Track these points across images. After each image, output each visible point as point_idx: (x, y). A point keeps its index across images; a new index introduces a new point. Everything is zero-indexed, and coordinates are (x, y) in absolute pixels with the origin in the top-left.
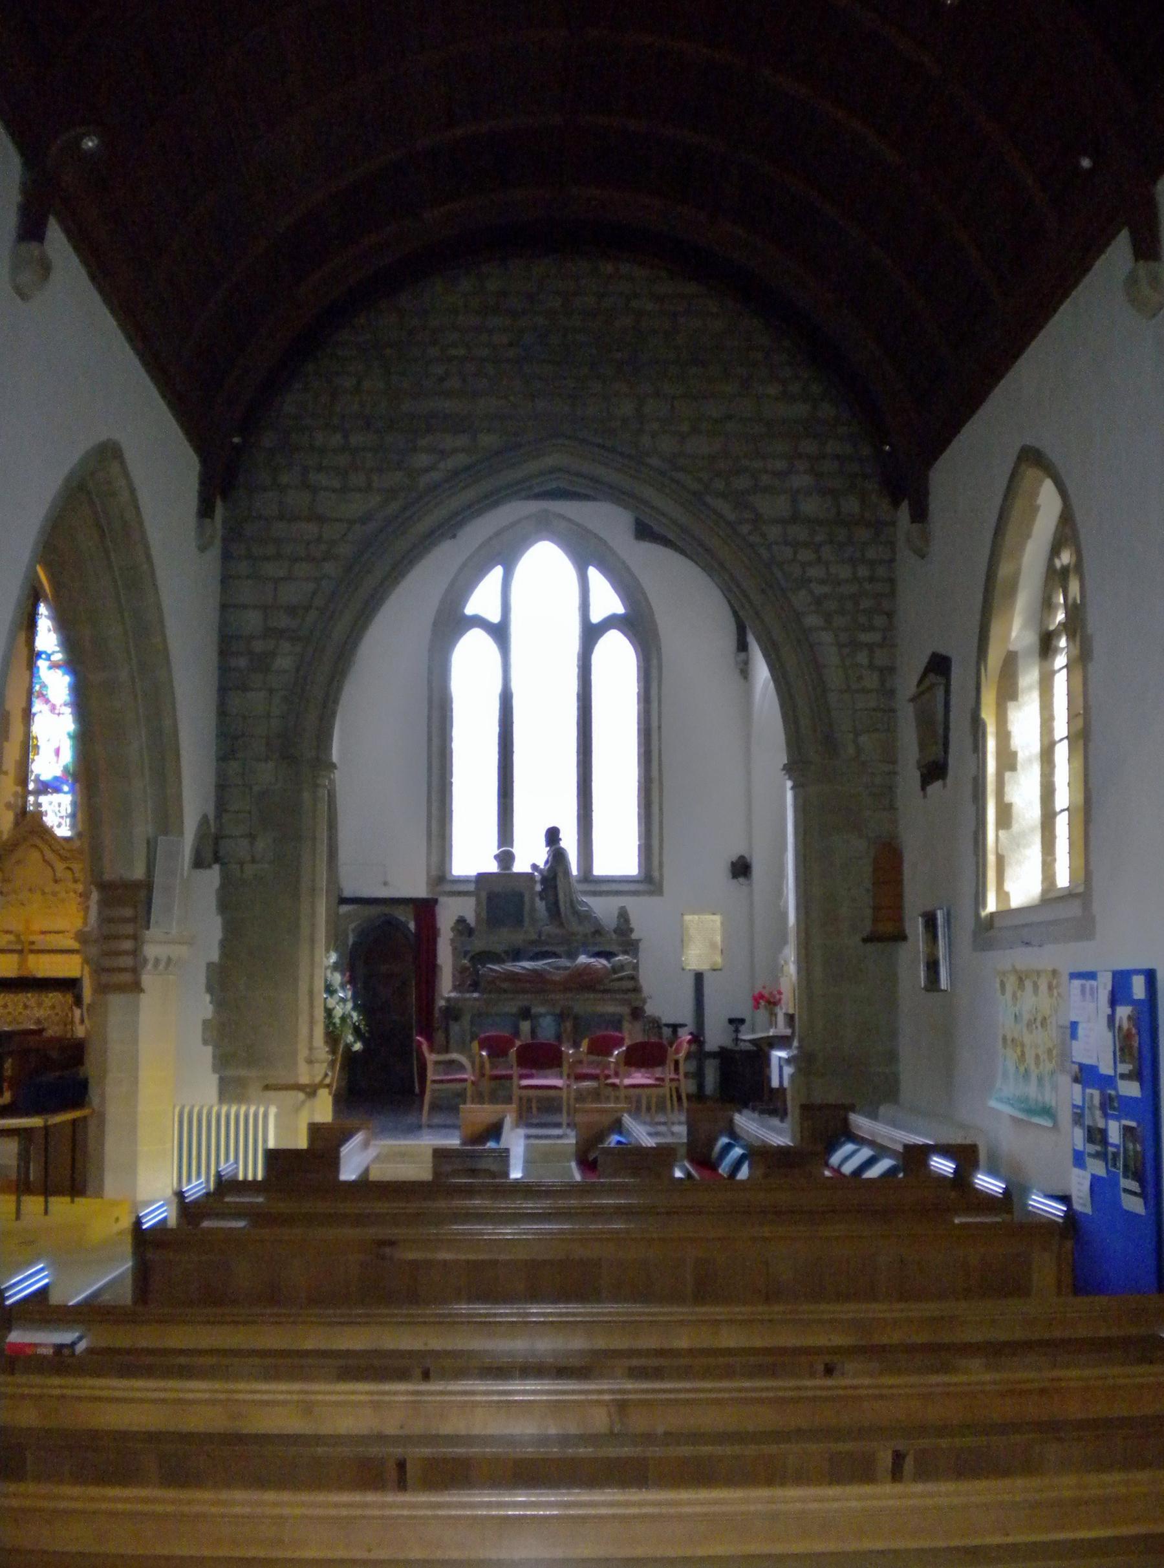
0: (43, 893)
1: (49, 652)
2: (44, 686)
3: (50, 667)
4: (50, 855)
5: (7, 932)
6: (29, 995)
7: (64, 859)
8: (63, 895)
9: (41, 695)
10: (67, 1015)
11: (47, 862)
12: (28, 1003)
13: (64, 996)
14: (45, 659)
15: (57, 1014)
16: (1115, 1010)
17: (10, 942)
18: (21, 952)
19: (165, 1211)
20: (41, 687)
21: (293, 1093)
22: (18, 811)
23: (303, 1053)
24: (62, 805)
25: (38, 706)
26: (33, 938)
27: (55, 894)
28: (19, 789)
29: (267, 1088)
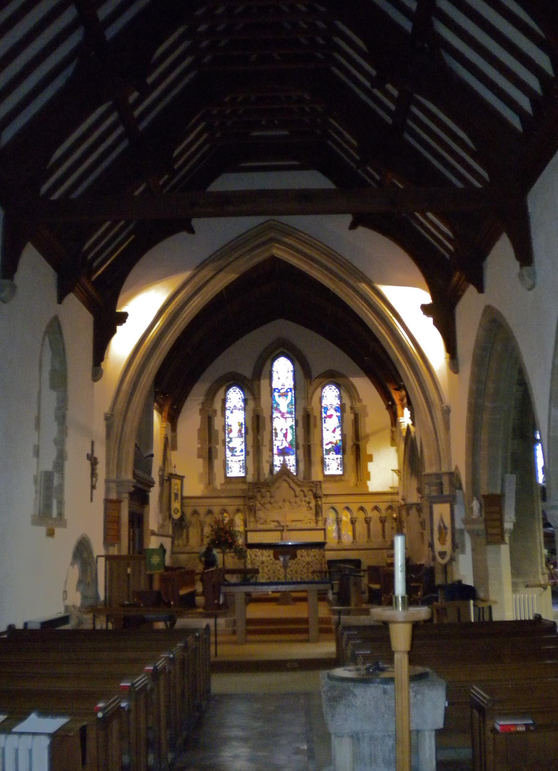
0: (290, 502)
1: (280, 388)
2: (278, 404)
3: (279, 396)
4: (292, 484)
5: (274, 521)
6: (303, 551)
7: (299, 486)
8: (299, 503)
9: (277, 409)
10: (322, 559)
11: (291, 487)
12: (303, 554)
13: (319, 551)
14: (277, 392)
15: (317, 559)
16: (217, 620)
17: (276, 526)
18: (282, 531)
19: (146, 680)
20: (277, 405)
21: (539, 588)
22: (271, 464)
23: (540, 570)
24: (290, 461)
25: (276, 414)
26: (288, 524)
27: (296, 502)
28: (271, 453)
29: (527, 586)
